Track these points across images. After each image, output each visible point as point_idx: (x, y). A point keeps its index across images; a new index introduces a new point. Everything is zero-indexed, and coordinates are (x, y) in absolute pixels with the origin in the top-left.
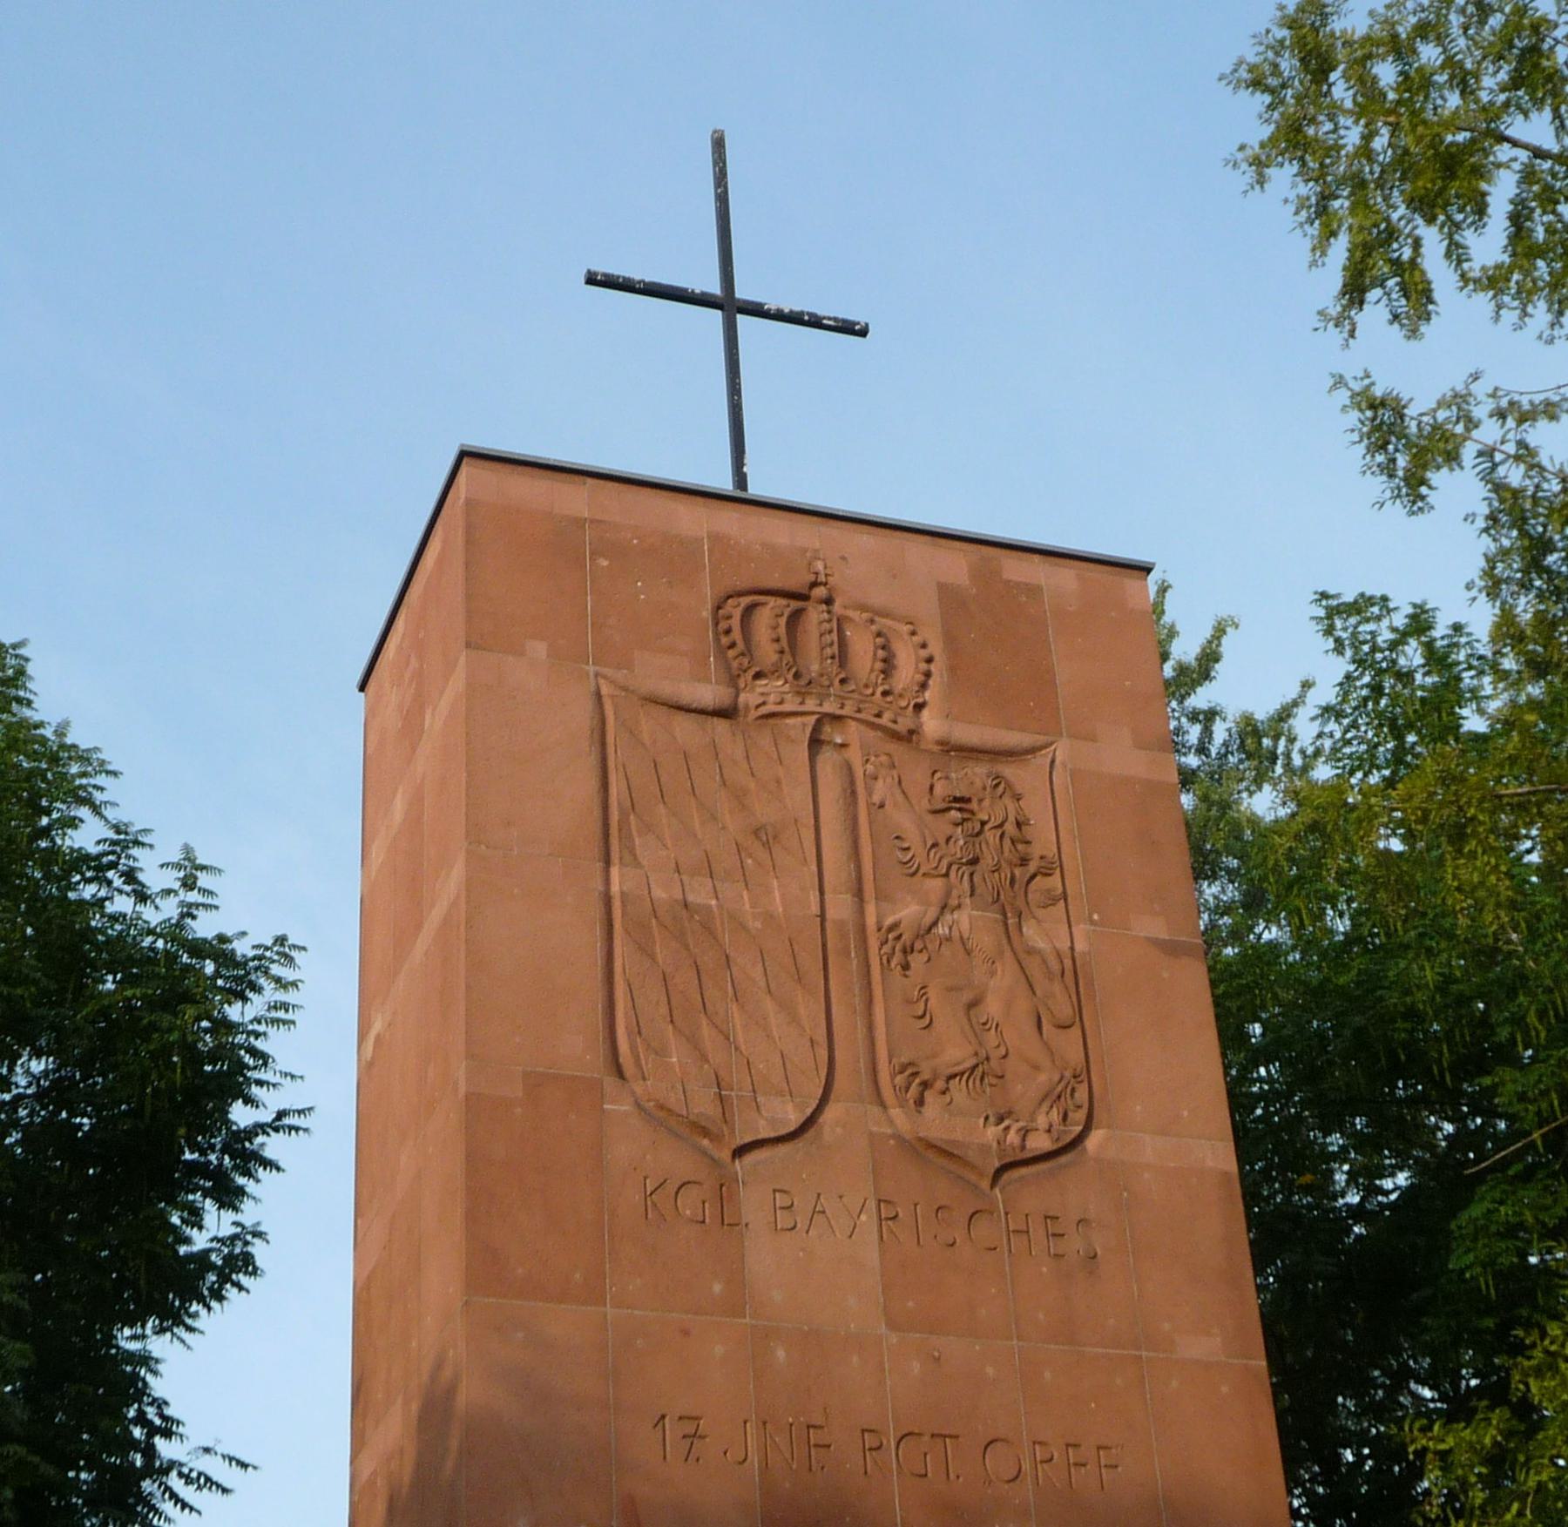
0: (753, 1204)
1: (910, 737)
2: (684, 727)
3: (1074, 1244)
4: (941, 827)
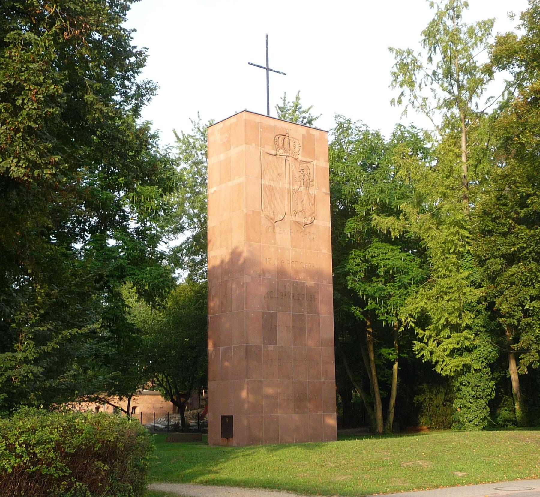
0: (277, 230)
1: (296, 159)
2: (271, 157)
3: (312, 236)
4: (300, 174)
